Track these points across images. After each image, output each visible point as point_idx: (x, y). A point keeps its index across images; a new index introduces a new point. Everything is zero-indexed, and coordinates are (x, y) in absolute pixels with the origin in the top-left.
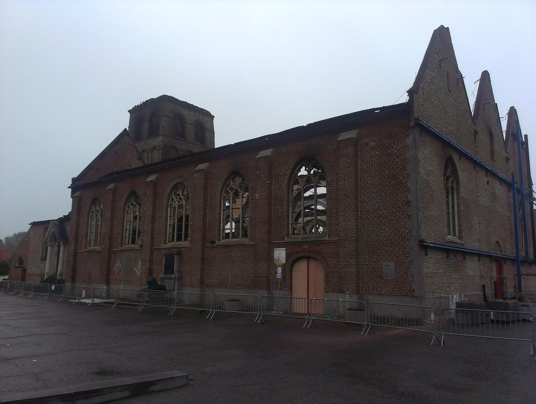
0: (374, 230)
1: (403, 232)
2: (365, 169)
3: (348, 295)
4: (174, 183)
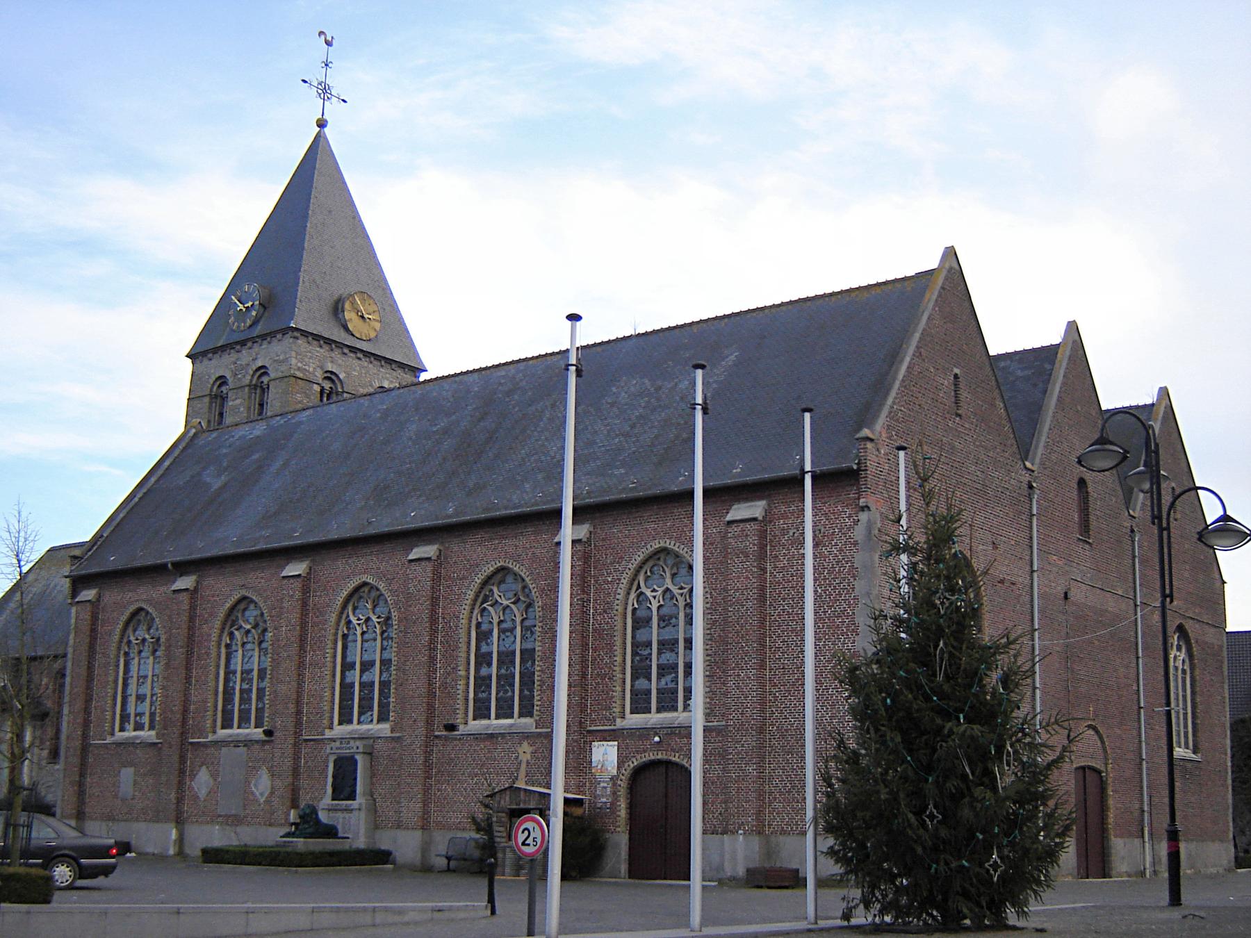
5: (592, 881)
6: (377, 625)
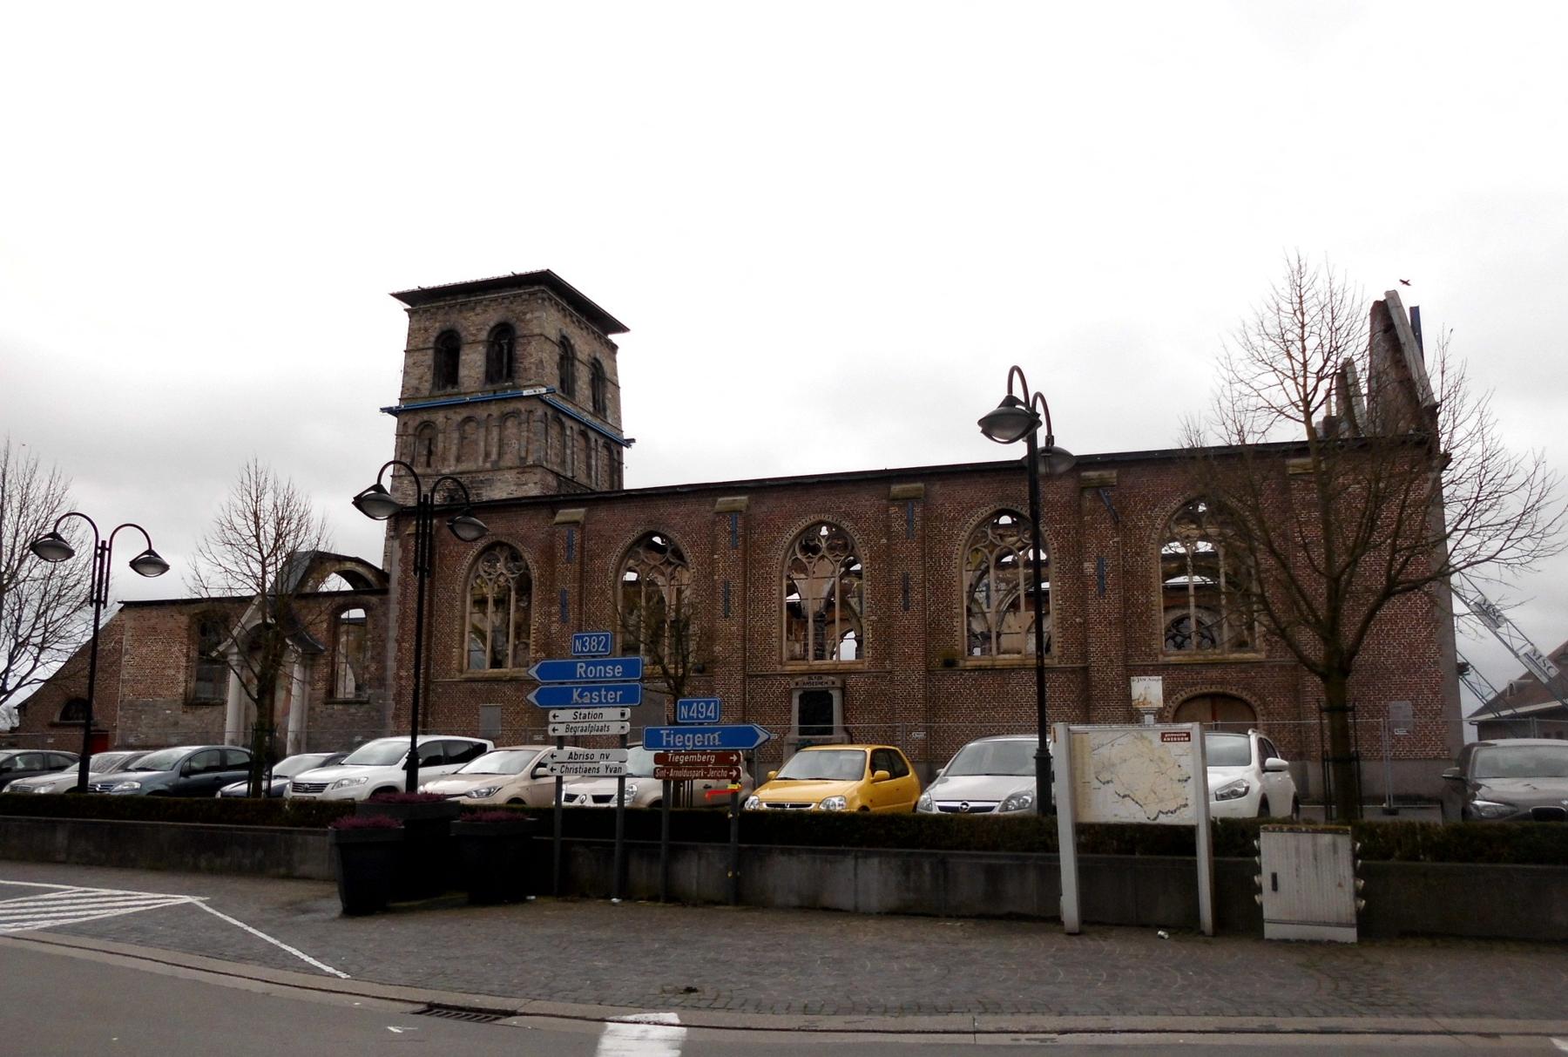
5: (1507, 803)
6: (511, 580)
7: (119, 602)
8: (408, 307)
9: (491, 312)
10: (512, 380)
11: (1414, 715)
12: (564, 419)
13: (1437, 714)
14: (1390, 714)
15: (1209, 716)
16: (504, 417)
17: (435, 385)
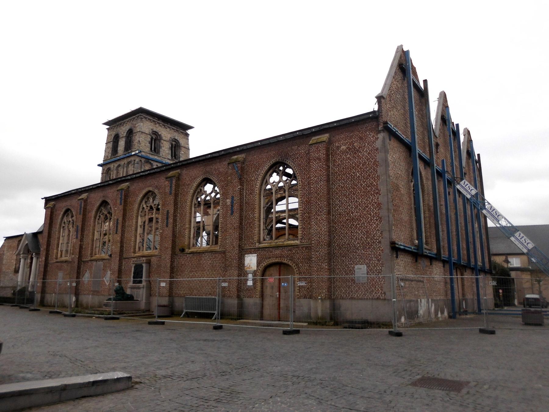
0: (347, 233)
1: (374, 234)
2: (336, 173)
3: (320, 301)
4: (144, 192)
7: (4, 237)
8: (108, 127)
9: (127, 126)
10: (131, 150)
11: (367, 273)
12: (152, 162)
13: (379, 272)
14: (356, 272)
15: (278, 275)
16: (129, 163)
17: (112, 154)
